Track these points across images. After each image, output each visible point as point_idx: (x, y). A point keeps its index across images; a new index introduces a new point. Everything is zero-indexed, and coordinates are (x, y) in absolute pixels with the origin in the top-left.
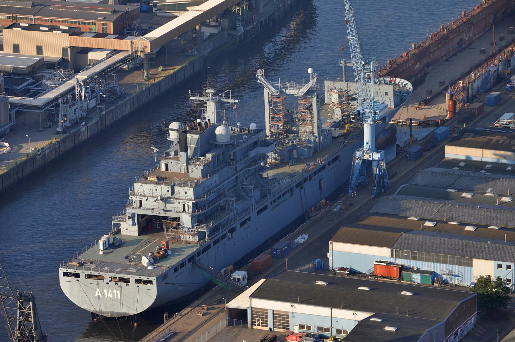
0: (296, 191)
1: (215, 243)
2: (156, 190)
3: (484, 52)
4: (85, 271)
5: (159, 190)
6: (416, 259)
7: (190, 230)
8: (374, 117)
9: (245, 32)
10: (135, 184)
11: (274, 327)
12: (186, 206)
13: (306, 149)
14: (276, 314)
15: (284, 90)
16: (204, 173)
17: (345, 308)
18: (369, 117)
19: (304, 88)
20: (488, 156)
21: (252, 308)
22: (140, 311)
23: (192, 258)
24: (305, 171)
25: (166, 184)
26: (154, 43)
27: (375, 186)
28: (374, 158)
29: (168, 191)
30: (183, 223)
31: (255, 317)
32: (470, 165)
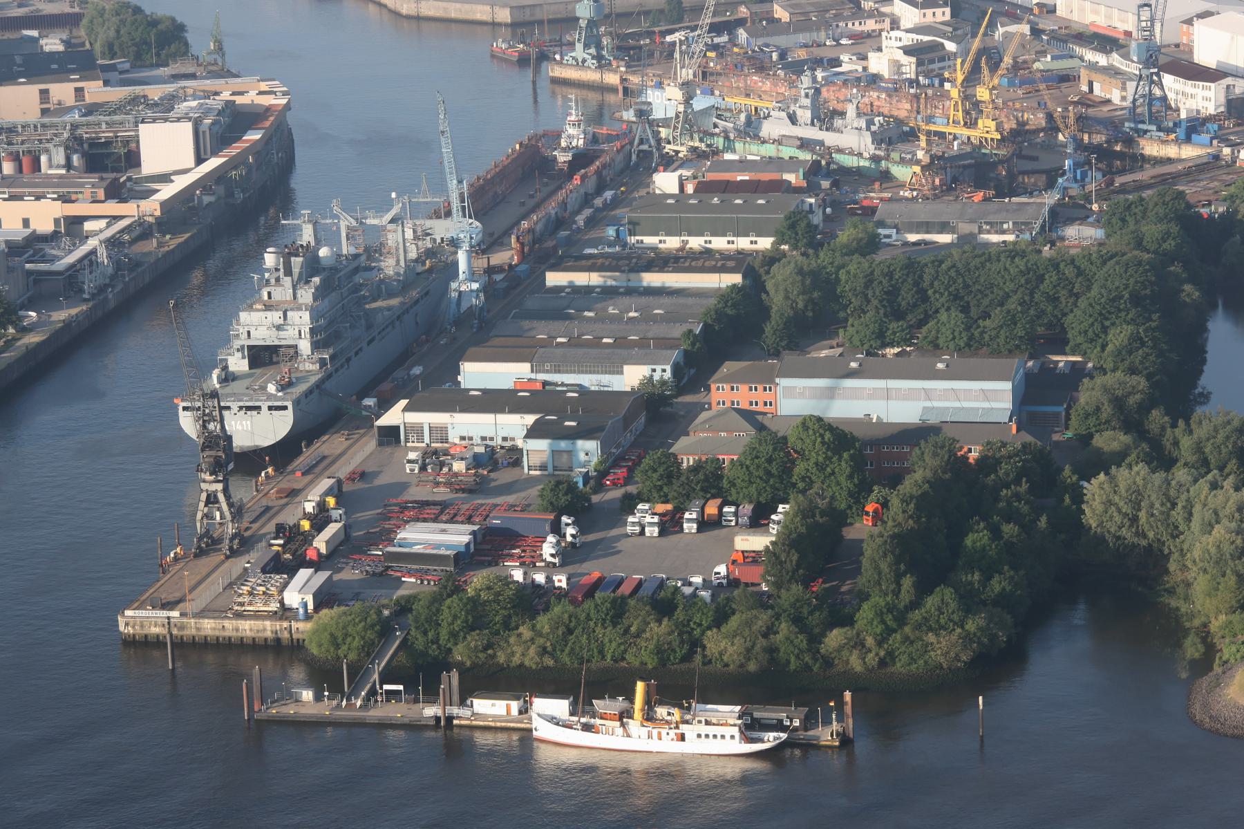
0: (398, 323)
1: (337, 370)
3: (523, 204)
5: (270, 318)
6: (559, 372)
16: (315, 299)
17: (511, 412)
20: (594, 279)
22: (279, 438)
23: (318, 385)
24: (402, 303)
26: (163, 204)
32: (576, 290)
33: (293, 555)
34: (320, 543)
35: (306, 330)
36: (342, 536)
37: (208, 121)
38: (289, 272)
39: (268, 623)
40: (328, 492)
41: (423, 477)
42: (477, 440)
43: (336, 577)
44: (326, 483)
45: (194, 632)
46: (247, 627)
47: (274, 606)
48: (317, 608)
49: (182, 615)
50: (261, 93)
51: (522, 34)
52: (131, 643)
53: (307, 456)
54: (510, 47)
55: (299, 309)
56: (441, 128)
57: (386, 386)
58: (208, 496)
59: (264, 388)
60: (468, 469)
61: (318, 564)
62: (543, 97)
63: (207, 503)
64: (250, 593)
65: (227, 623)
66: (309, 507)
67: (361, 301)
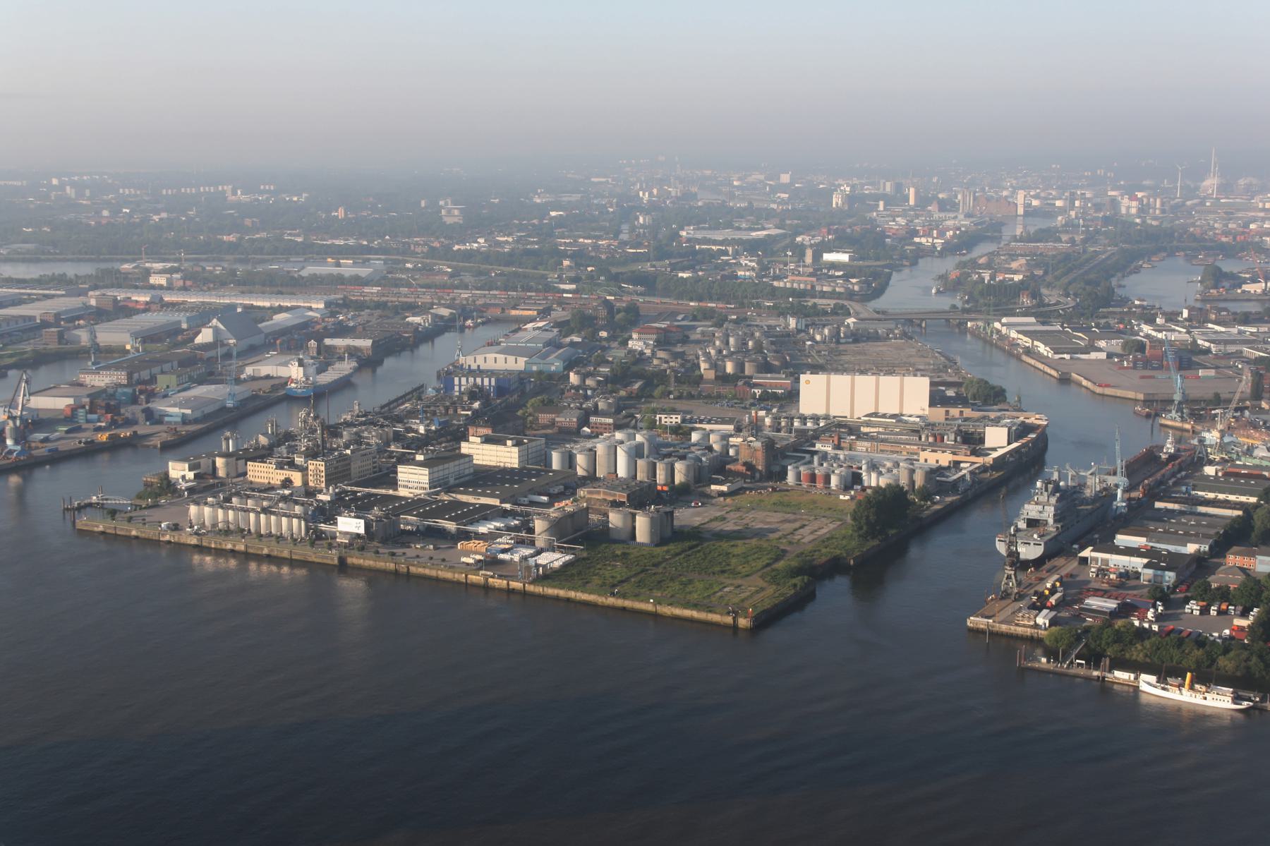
20: (1176, 507)
23: (1055, 537)
32: (1167, 510)
34: (1053, 600)
44: (1056, 577)
52: (971, 630)
53: (1048, 565)
57: (1082, 541)
61: (1052, 608)
66: (1049, 585)
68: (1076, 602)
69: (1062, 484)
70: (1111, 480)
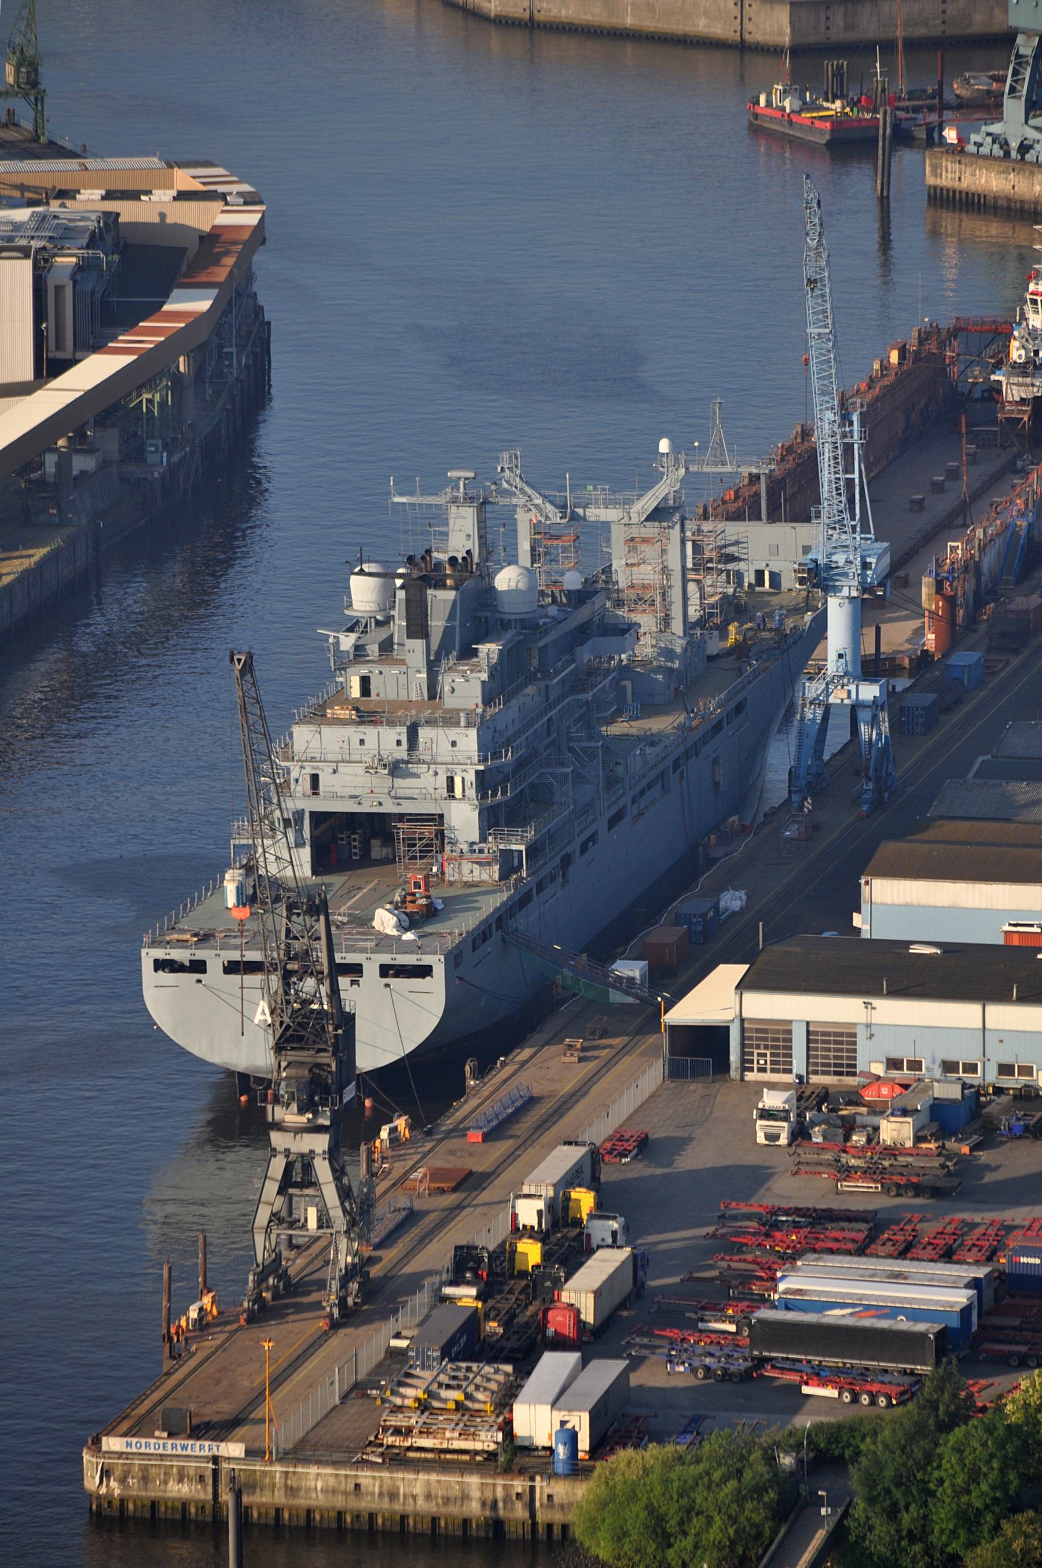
0: (674, 777)
1: (540, 886)
2: (362, 742)
3: (919, 506)
4: (222, 952)
5: (371, 743)
7: (476, 847)
8: (863, 575)
9: (172, 469)
10: (296, 730)
11: (808, 1073)
12: (458, 781)
13: (660, 677)
14: (816, 1033)
15: (580, 511)
18: (845, 575)
19: (645, 499)
21: (742, 1020)
23: (500, 920)
24: (684, 729)
25: (391, 723)
27: (869, 779)
28: (861, 697)
29: (399, 743)
30: (452, 829)
31: (751, 1046)
33: (507, 1324)
34: (580, 1294)
35: (466, 777)
36: (628, 1285)
37: (66, 261)
38: (418, 627)
39: (473, 1481)
40: (573, 1179)
41: (807, 1155)
42: (930, 1069)
43: (635, 1379)
44: (565, 1158)
45: (279, 1498)
46: (418, 1489)
47: (488, 1440)
48: (601, 1446)
49: (251, 1453)
50: (183, 196)
51: (838, 73)
52: (113, 1520)
53: (483, 1096)
54: (806, 107)
55: (450, 720)
56: (808, 272)
57: (664, 933)
58: (289, 1168)
59: (364, 921)
60: (918, 1139)
61: (590, 1342)
62: (909, 234)
63: (286, 1184)
64: (423, 1406)
65: (367, 1478)
66: (528, 1212)
67: (590, 718)
68: (715, 1296)
69: (506, 579)
70: (773, 549)
